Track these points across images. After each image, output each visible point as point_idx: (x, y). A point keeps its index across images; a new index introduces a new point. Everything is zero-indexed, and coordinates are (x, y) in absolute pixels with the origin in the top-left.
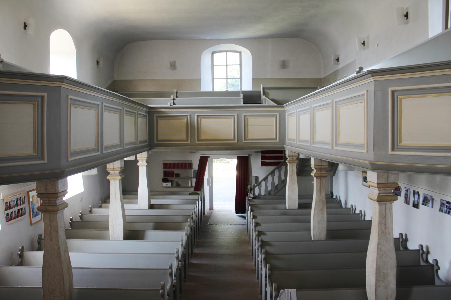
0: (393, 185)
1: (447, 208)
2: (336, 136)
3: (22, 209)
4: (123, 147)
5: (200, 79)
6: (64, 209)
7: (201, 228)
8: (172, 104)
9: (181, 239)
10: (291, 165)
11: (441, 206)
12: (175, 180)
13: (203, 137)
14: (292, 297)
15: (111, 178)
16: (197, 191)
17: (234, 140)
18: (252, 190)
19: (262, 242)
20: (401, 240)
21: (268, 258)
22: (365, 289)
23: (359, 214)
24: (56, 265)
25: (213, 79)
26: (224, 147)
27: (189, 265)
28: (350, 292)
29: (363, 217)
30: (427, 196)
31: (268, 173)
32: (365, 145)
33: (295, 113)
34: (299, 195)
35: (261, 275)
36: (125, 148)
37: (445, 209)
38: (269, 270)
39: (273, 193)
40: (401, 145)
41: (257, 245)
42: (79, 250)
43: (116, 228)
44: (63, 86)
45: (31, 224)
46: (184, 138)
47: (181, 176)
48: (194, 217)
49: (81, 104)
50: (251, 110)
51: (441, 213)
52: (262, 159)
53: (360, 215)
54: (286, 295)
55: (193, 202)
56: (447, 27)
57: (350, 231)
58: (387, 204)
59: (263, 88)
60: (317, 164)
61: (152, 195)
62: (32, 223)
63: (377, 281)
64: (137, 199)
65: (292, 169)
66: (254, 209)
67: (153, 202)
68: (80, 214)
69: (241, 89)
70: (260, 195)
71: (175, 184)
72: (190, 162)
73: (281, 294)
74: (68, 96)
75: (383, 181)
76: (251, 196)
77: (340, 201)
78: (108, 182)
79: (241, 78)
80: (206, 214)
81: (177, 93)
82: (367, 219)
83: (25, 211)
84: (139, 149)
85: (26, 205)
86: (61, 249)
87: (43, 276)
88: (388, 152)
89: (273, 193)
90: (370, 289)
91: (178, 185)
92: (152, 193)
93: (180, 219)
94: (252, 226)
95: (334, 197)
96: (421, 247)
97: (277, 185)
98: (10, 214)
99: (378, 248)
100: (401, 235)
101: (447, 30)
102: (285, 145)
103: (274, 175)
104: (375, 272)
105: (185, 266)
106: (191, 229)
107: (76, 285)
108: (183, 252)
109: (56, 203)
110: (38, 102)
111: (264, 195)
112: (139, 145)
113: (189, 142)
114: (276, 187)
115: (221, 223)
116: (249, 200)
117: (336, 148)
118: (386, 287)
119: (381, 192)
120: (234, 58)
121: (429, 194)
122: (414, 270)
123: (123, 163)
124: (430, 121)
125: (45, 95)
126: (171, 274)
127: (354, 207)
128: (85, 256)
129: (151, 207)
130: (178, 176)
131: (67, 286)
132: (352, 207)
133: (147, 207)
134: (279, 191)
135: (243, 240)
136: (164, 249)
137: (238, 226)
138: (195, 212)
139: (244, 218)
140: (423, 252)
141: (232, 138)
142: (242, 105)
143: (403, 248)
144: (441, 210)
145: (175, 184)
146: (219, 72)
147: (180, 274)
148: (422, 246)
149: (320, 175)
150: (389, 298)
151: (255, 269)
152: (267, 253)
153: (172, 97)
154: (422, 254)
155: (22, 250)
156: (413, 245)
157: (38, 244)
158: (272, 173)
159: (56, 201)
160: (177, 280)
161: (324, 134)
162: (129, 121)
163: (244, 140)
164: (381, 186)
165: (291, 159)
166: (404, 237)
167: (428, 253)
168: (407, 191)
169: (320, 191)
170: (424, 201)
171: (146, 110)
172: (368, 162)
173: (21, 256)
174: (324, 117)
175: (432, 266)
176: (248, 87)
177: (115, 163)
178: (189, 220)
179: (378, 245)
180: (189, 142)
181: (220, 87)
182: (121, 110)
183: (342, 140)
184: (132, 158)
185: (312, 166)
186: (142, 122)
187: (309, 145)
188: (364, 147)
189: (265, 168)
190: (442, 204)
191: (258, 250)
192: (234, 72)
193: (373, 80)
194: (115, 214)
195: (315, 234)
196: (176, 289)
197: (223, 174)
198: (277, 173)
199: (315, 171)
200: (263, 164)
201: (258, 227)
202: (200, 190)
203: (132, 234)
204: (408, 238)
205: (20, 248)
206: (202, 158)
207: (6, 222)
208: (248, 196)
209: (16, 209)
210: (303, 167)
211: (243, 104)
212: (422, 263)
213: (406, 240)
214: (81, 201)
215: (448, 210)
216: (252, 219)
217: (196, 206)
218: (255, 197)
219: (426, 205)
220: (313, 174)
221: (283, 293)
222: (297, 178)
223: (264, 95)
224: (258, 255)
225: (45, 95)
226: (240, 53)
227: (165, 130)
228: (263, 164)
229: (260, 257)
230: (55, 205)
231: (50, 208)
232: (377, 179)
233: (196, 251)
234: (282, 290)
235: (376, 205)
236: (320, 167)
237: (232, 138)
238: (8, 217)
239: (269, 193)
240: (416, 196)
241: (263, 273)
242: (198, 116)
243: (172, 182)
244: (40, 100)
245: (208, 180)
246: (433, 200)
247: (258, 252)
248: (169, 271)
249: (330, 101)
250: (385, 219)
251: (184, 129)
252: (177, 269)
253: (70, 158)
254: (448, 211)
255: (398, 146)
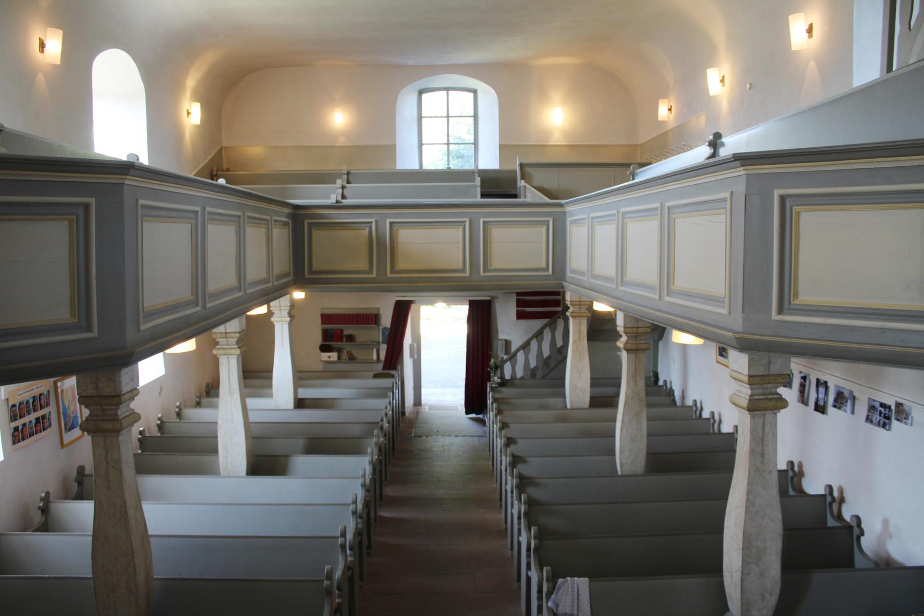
0: (780, 378)
1: (880, 415)
2: (668, 275)
3: (43, 417)
4: (245, 291)
5: (395, 146)
6: (133, 424)
7: (399, 440)
8: (339, 198)
9: (361, 473)
10: (577, 321)
11: (869, 411)
12: (346, 346)
13: (401, 265)
14: (581, 598)
15: (220, 352)
16: (389, 369)
17: (464, 271)
18: (499, 367)
19: (521, 477)
20: (790, 474)
21: (534, 511)
22: (722, 576)
23: (709, 419)
24: (118, 527)
25: (421, 144)
26: (442, 284)
27: (376, 522)
28: (691, 584)
29: (716, 425)
30: (842, 390)
31: (531, 334)
32: (727, 300)
33: (585, 219)
34: (592, 379)
35: (519, 544)
36: (249, 291)
37: (876, 417)
38: (535, 538)
39: (539, 373)
40: (797, 302)
41: (510, 483)
42: (159, 497)
43: (233, 450)
44: (126, 182)
45: (63, 445)
46: (364, 266)
47: (358, 340)
48: (386, 425)
49: (163, 213)
50: (499, 210)
51: (869, 425)
52: (518, 306)
53: (712, 421)
54: (570, 590)
55: (382, 393)
56: (889, 68)
57: (692, 456)
58: (767, 416)
59: (521, 165)
60: (628, 325)
61: (300, 379)
62: (65, 442)
63: (745, 563)
64: (271, 386)
65: (577, 330)
66: (503, 407)
67: (304, 393)
68: (159, 419)
69: (477, 166)
70: (513, 377)
71: (344, 356)
72: (375, 312)
73: (560, 588)
74: (137, 200)
75: (760, 371)
76: (496, 379)
77: (671, 392)
78: (216, 361)
79: (476, 143)
80: (407, 414)
81: (348, 174)
82: (726, 428)
83: (49, 419)
84: (275, 291)
85: (51, 410)
86: (128, 505)
87: (93, 557)
88: (770, 315)
89: (539, 373)
90: (732, 577)
91: (352, 358)
92: (301, 376)
93: (357, 430)
94: (499, 443)
95: (661, 383)
96: (828, 490)
97: (549, 357)
98: (20, 428)
99: (748, 500)
100: (791, 463)
101: (891, 75)
102: (565, 281)
103: (542, 339)
104: (741, 546)
105: (368, 524)
106: (380, 450)
107: (159, 572)
108: (366, 496)
109: (116, 415)
110: (77, 216)
111: (522, 378)
112: (276, 283)
113: (374, 275)
114: (546, 362)
115: (438, 433)
116: (492, 389)
117: (667, 299)
118: (761, 575)
119: (755, 392)
120: (462, 102)
121: (847, 386)
122: (818, 536)
123: (244, 321)
124: (852, 257)
125: (92, 201)
126: (343, 547)
127: (698, 405)
128: (173, 510)
129: (300, 404)
130: (350, 338)
131: (141, 578)
132: (696, 405)
133: (290, 404)
134: (552, 370)
135: (480, 468)
136: (326, 492)
137: (470, 439)
138: (386, 415)
139: (482, 422)
140: (832, 500)
141: (460, 266)
142: (479, 199)
143: (794, 489)
144: (869, 419)
145: (344, 356)
146: (433, 131)
147: (360, 543)
148: (830, 488)
149: (634, 347)
150: (767, 595)
151: (506, 528)
152: (530, 502)
153: (339, 182)
154: (831, 504)
155: (46, 500)
156: (814, 486)
157: (79, 487)
158: (539, 335)
159: (116, 410)
160: (354, 555)
161: (643, 267)
162: (255, 236)
163: (484, 271)
164: (756, 380)
165: (577, 309)
166: (796, 469)
167: (842, 500)
168: (804, 378)
169: (633, 377)
170: (836, 400)
171: (287, 210)
172: (730, 334)
173: (45, 511)
174: (644, 235)
175: (849, 527)
176: (489, 160)
177: (228, 324)
178: (376, 432)
179: (748, 494)
180: (374, 275)
181: (434, 160)
182: (239, 217)
183: (680, 283)
184: (262, 310)
185: (618, 329)
186: (281, 236)
187: (614, 286)
188: (724, 302)
189: (524, 323)
190: (872, 408)
191: (512, 492)
192: (463, 130)
193: (743, 173)
194: (229, 422)
195: (624, 461)
196: (353, 574)
197: (440, 334)
198: (547, 334)
199: (624, 338)
200: (520, 316)
201: (512, 446)
202: (395, 368)
203: (264, 463)
204: (805, 469)
205: (43, 495)
206: (398, 303)
207: (14, 443)
208: (489, 381)
209: (32, 417)
210: (600, 329)
211: (483, 196)
212: (831, 522)
213: (801, 474)
214: (160, 394)
215: (883, 420)
216: (496, 416)
217: (387, 401)
218: (504, 383)
219: (839, 408)
220: (620, 343)
221: (562, 584)
222: (589, 347)
223: (522, 179)
224: (512, 503)
225: (92, 201)
226: (475, 92)
227: (325, 249)
228: (520, 316)
229: (516, 508)
230: (116, 419)
231: (106, 425)
232: (749, 366)
233: (389, 491)
234: (561, 580)
235: (747, 416)
236: (635, 330)
237: (460, 266)
238: (16, 433)
239: (533, 373)
240: (822, 390)
241: (524, 539)
242: (391, 223)
243: (339, 351)
244: (81, 211)
245: (411, 346)
246: (854, 398)
247: (512, 497)
248: (340, 540)
249: (657, 205)
250: (763, 441)
251: (364, 250)
252: (354, 534)
253: (145, 323)
254: (881, 423)
255: (790, 303)
